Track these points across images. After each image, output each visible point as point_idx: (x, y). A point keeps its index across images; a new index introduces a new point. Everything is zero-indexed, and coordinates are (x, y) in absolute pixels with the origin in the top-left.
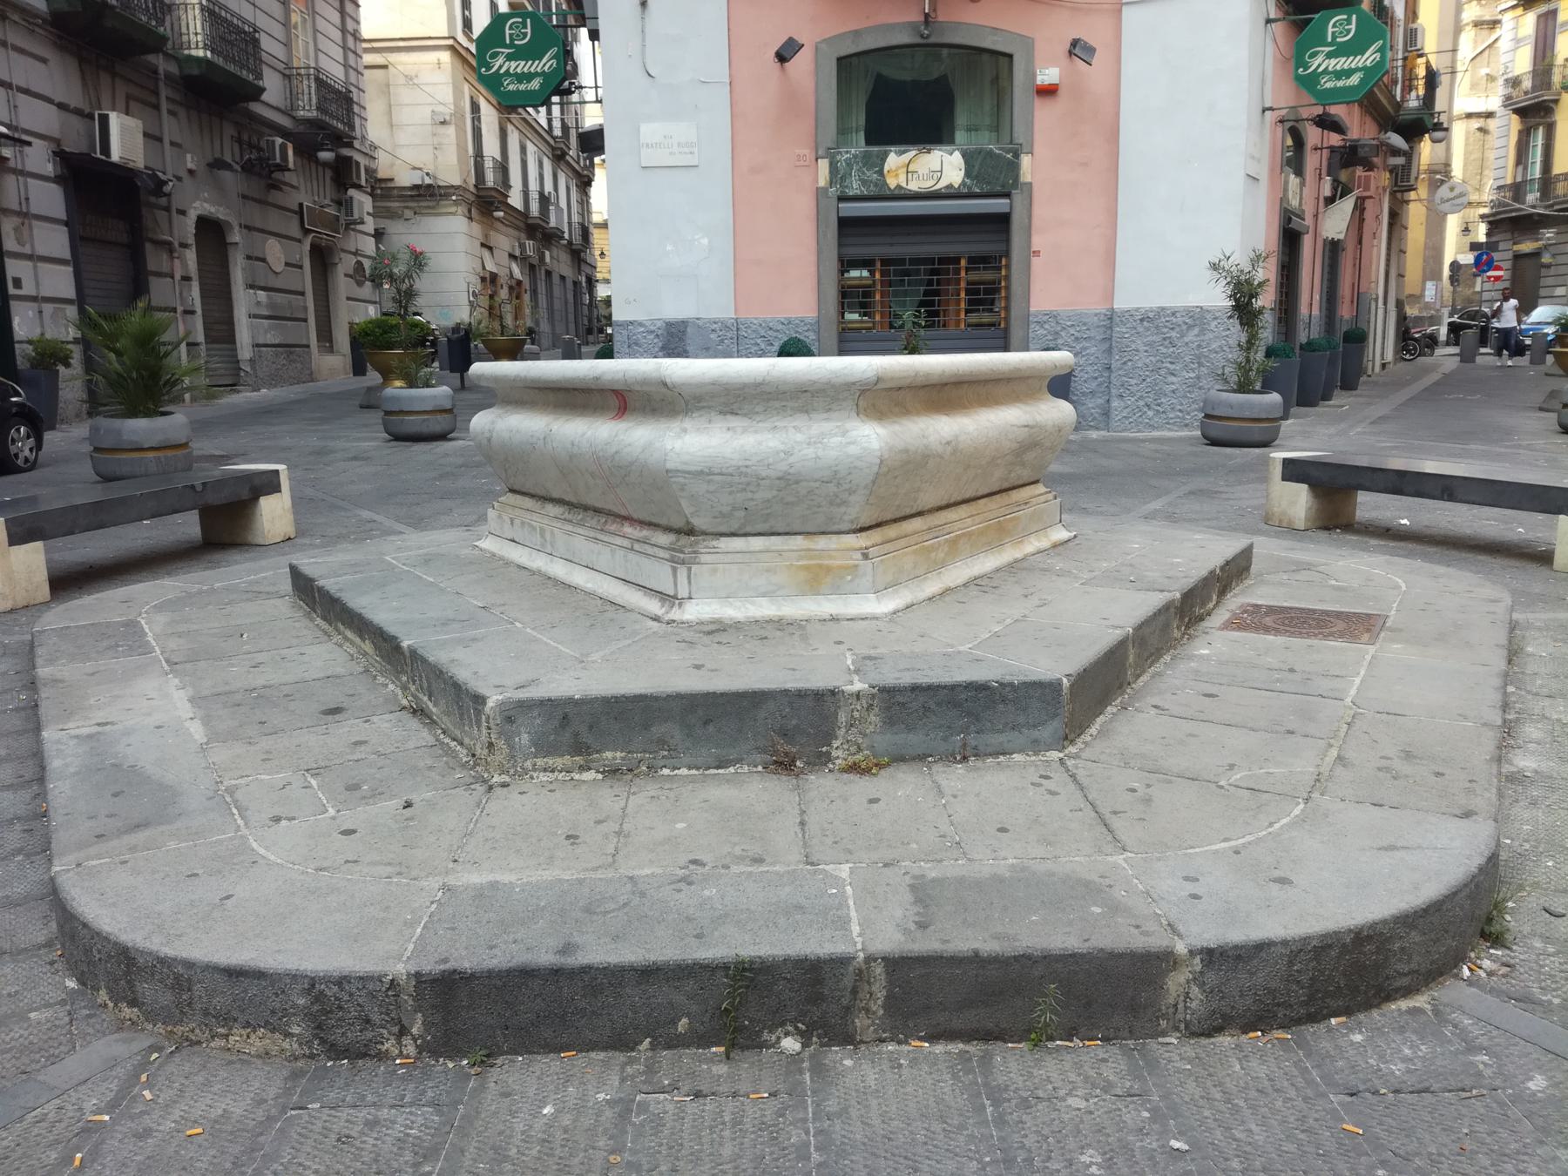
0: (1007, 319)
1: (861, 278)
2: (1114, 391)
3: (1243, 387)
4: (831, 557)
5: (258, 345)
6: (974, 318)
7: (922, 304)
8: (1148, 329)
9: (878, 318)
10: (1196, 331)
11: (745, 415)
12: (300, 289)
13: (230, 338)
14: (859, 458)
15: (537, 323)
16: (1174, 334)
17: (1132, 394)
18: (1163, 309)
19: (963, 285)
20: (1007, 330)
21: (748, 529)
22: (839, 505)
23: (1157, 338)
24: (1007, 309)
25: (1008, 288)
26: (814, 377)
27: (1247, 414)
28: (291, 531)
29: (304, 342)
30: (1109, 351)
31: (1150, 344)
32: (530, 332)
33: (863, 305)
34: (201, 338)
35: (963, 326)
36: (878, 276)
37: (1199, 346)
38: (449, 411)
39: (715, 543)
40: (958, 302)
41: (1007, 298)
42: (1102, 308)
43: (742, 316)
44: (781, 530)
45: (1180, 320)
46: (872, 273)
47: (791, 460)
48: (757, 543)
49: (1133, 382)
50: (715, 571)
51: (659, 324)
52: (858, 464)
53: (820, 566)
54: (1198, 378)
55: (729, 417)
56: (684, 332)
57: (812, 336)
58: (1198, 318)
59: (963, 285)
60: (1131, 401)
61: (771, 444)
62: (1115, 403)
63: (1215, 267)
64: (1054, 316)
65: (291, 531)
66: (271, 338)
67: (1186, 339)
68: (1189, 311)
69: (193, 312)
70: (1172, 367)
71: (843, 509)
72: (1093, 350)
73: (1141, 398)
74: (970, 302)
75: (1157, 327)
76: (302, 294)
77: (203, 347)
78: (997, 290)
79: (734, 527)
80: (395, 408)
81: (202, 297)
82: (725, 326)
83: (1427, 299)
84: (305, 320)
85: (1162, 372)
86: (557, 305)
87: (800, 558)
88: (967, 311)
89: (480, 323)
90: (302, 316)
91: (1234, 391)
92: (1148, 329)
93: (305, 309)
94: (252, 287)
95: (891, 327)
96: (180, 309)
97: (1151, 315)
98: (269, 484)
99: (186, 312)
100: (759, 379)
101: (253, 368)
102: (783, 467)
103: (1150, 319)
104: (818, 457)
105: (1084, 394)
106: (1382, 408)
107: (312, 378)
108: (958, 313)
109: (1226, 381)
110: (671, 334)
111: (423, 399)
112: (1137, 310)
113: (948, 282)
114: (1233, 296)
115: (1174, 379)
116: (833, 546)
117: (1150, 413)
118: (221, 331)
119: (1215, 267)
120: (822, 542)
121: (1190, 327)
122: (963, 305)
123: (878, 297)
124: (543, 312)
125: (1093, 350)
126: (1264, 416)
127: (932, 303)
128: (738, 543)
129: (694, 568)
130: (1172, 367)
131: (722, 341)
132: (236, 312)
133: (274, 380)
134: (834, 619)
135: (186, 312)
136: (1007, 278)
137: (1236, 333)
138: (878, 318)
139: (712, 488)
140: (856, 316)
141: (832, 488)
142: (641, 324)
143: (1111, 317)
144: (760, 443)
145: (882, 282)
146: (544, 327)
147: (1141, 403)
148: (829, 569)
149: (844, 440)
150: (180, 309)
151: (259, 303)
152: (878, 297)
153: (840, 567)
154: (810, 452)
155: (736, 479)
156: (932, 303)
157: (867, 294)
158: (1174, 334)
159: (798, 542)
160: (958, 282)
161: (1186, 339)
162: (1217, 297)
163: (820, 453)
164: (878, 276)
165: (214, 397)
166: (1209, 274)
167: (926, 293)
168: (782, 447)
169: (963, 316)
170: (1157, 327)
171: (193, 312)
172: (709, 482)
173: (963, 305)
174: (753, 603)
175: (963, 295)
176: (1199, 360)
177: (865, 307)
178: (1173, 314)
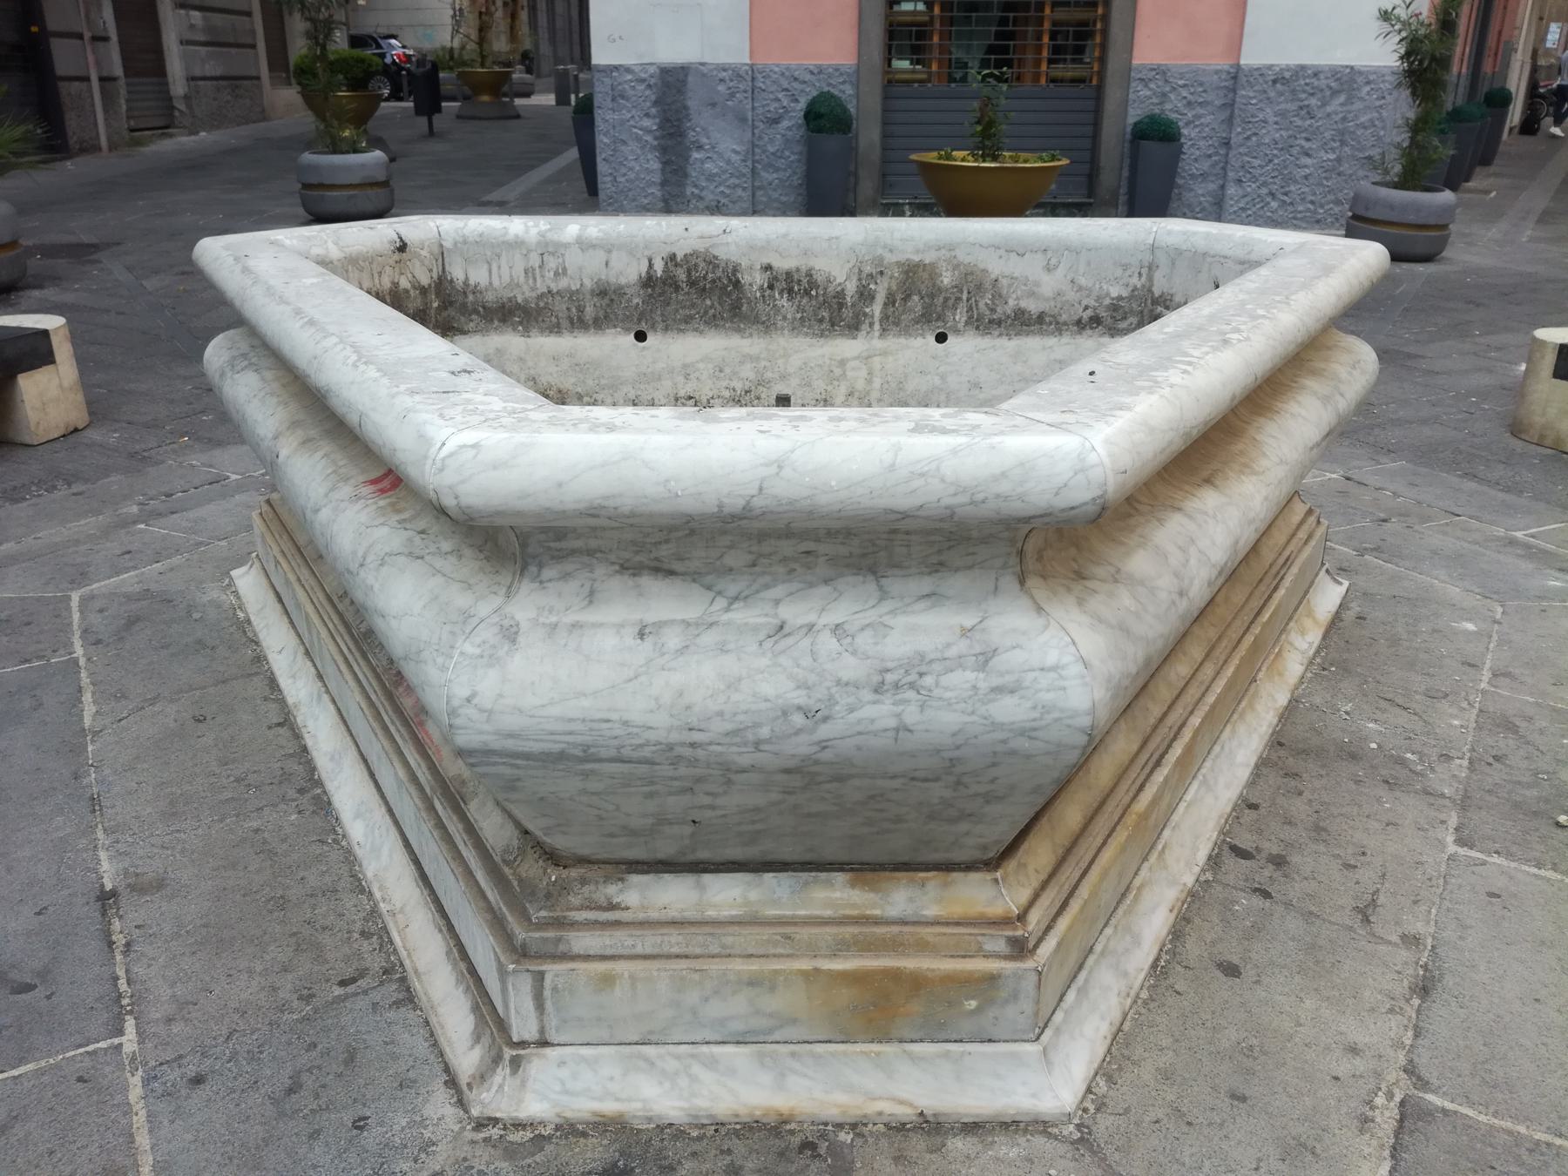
0: (1101, 75)
1: (915, 13)
2: (1231, 174)
3: (1408, 180)
4: (923, 947)
5: (194, 79)
6: (1060, 71)
7: (991, 50)
8: (1281, 94)
9: (934, 67)
10: (1342, 98)
11: (695, 577)
12: (245, 8)
13: (160, 71)
14: (1027, 732)
15: (536, 45)
16: (1313, 101)
17: (1254, 179)
18: (1303, 68)
19: (1047, 25)
20: (1100, 88)
21: (703, 854)
22: (953, 821)
23: (1292, 106)
24: (1102, 60)
25: (1105, 32)
26: (904, 503)
27: (1411, 218)
28: (79, 416)
29: (254, 74)
30: (1230, 121)
31: (1283, 114)
32: (525, 57)
33: (916, 50)
34: (118, 71)
35: (1043, 81)
36: (937, 10)
37: (1344, 119)
38: (385, 184)
39: (611, 890)
40: (1039, 49)
41: (1104, 47)
42: (1223, 63)
43: (760, 61)
44: (787, 852)
45: (1323, 83)
46: (930, 6)
47: (824, 731)
48: (727, 894)
49: (1256, 162)
50: (608, 980)
51: (652, 70)
52: (1023, 744)
53: (895, 975)
54: (1339, 160)
55: (646, 581)
56: (684, 82)
57: (849, 90)
58: (1347, 81)
59: (1047, 25)
60: (1250, 187)
61: (768, 689)
62: (1232, 190)
63: (1385, 16)
64: (1161, 71)
65: (79, 416)
66: (212, 69)
67: (1329, 109)
68: (1335, 72)
69: (106, 39)
70: (1307, 145)
71: (963, 827)
72: (1209, 119)
73: (1265, 184)
74: (1056, 50)
75: (1293, 91)
76: (249, 14)
77: (122, 82)
78: (1089, 35)
79: (665, 850)
80: (314, 180)
81: (116, 18)
82: (736, 73)
83: (1549, 45)
84: (254, 46)
85: (1294, 151)
86: (559, 23)
87: (840, 948)
88: (1050, 61)
89: (463, 48)
90: (249, 41)
91: (1396, 186)
92: (1281, 94)
93: (253, 32)
94: (182, 6)
95: (951, 79)
96: (87, 35)
97: (1287, 75)
98: (37, 350)
99: (95, 39)
100: (735, 504)
101: (189, 107)
102: (801, 747)
103: (1288, 81)
104: (902, 728)
105: (1192, 176)
106: (1537, 198)
107: (263, 116)
108: (1038, 63)
109: (1386, 172)
110: (666, 85)
111: (348, 168)
112: (1270, 67)
113: (1026, 21)
114: (1406, 57)
115: (1308, 161)
116: (931, 911)
117: (1274, 204)
118: (145, 58)
119: (1385, 16)
120: (901, 899)
121: (1335, 93)
122: (1045, 54)
123: (936, 39)
124: (544, 34)
125: (1209, 119)
126: (1432, 221)
127: (1005, 50)
128: (672, 895)
129: (552, 970)
130: (1307, 145)
131: (732, 95)
132: (164, 37)
133: (216, 120)
134: (932, 1127)
135: (95, 39)
136: (1106, 18)
137: (1402, 107)
138: (934, 67)
139: (594, 785)
140: (905, 64)
141: (938, 791)
142: (628, 70)
143: (1236, 77)
144: (733, 685)
145: (942, 18)
146: (545, 49)
147: (1264, 191)
148: (916, 983)
149: (984, 682)
150: (87, 35)
151: (192, 26)
152: (936, 39)
153: (950, 979)
154: (880, 713)
155: (666, 770)
156: (1005, 50)
157: (921, 35)
158: (1313, 101)
159: (836, 895)
160: (1040, 22)
161: (1329, 109)
162: (1381, 54)
163: (911, 715)
164: (937, 10)
165: (138, 143)
166: (1379, 26)
167: (999, 35)
168: (799, 698)
169: (1044, 67)
170: (1293, 91)
171: (106, 39)
172: (586, 775)
173: (1045, 54)
174: (712, 1063)
175: (1046, 39)
176: (1342, 137)
177: (917, 52)
178: (1316, 75)
